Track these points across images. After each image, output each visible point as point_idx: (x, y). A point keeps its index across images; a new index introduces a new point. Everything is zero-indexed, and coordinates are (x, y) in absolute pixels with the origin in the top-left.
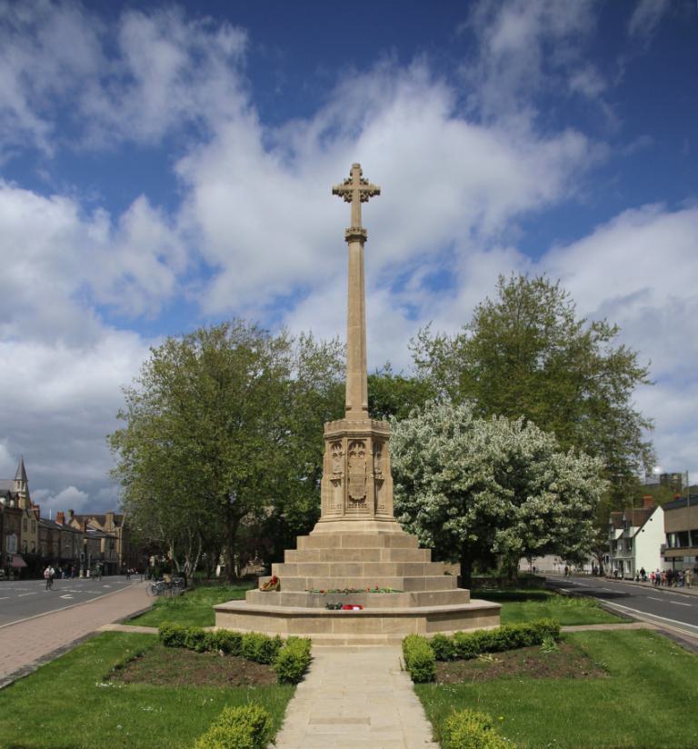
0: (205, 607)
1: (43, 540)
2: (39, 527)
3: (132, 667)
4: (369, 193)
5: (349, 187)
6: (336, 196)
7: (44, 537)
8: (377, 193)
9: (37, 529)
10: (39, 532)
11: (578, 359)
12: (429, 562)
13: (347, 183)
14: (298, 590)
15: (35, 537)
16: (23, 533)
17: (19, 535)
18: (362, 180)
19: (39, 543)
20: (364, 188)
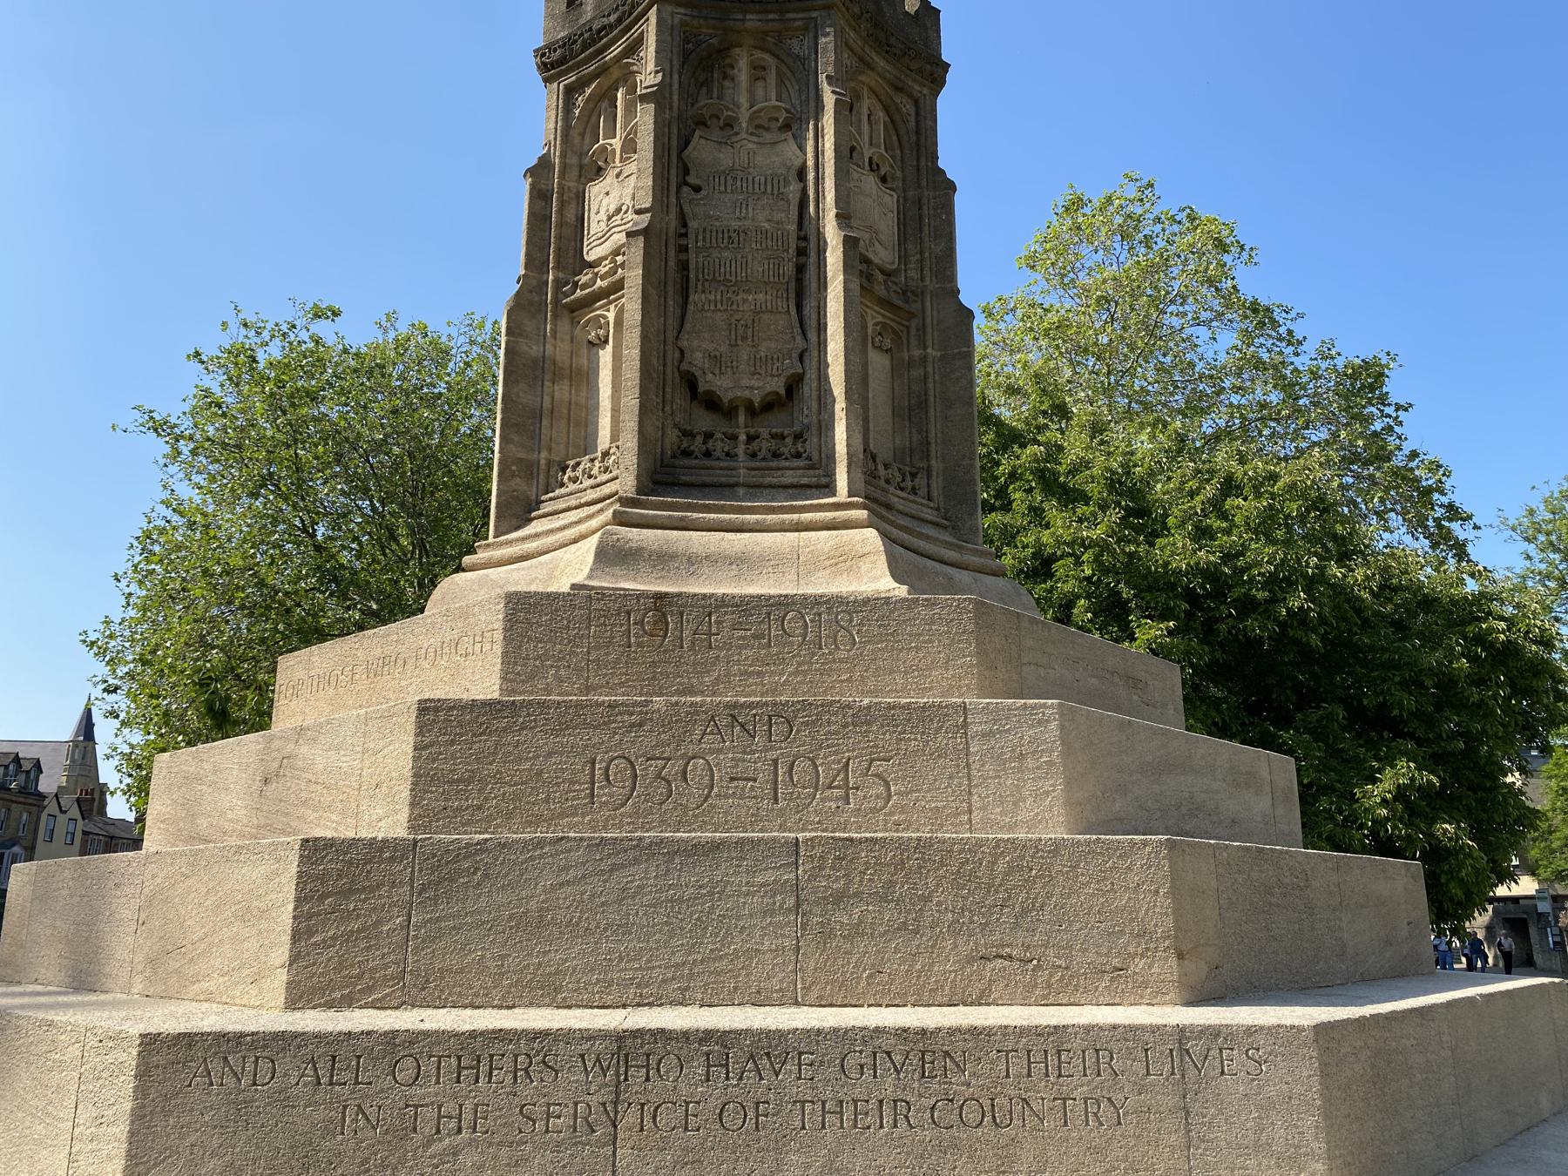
2: (85, 833)
9: (79, 835)
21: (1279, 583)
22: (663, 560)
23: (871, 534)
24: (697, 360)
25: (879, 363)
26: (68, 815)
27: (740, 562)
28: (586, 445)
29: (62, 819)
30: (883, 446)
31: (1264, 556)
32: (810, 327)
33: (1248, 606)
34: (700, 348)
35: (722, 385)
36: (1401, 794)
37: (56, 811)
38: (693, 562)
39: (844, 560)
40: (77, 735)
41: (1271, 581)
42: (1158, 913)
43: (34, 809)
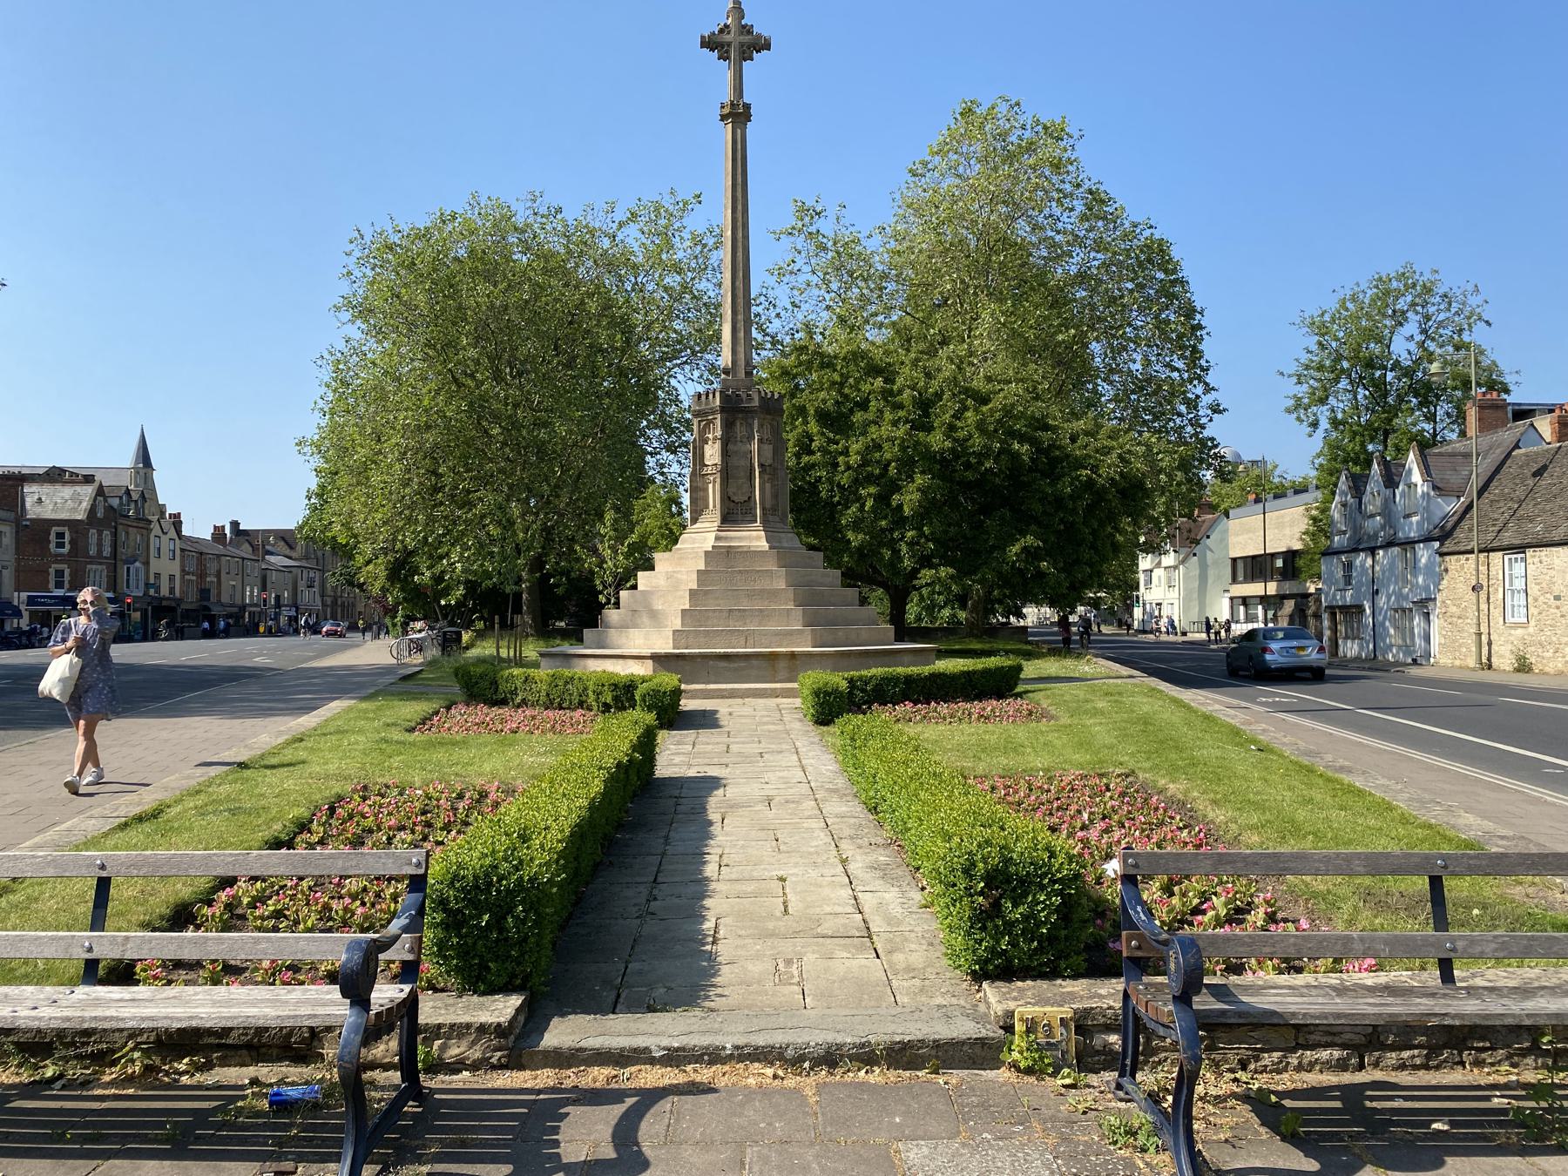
0: (590, 562)
1: (188, 574)
2: (182, 550)
3: (178, 793)
4: (755, 45)
5: (727, 38)
6: (705, 50)
7: (192, 566)
8: (767, 46)
9: (178, 552)
10: (182, 557)
11: (455, 758)
12: (1430, 932)
13: (721, 31)
14: (751, 498)
15: (175, 568)
16: (153, 561)
17: (147, 563)
18: (744, 27)
19: (182, 577)
20: (747, 38)
21: (983, 455)
22: (726, 538)
23: (583, 1159)
24: (730, 494)
25: (768, 486)
26: (169, 536)
27: (740, 539)
28: (707, 507)
29: (165, 538)
30: (768, 506)
31: (978, 442)
32: (752, 486)
33: (968, 466)
34: (731, 490)
35: (735, 498)
36: (1025, 549)
37: (160, 534)
38: (731, 539)
39: (758, 538)
40: (137, 462)
41: (979, 455)
42: (792, 596)
43: (144, 532)
